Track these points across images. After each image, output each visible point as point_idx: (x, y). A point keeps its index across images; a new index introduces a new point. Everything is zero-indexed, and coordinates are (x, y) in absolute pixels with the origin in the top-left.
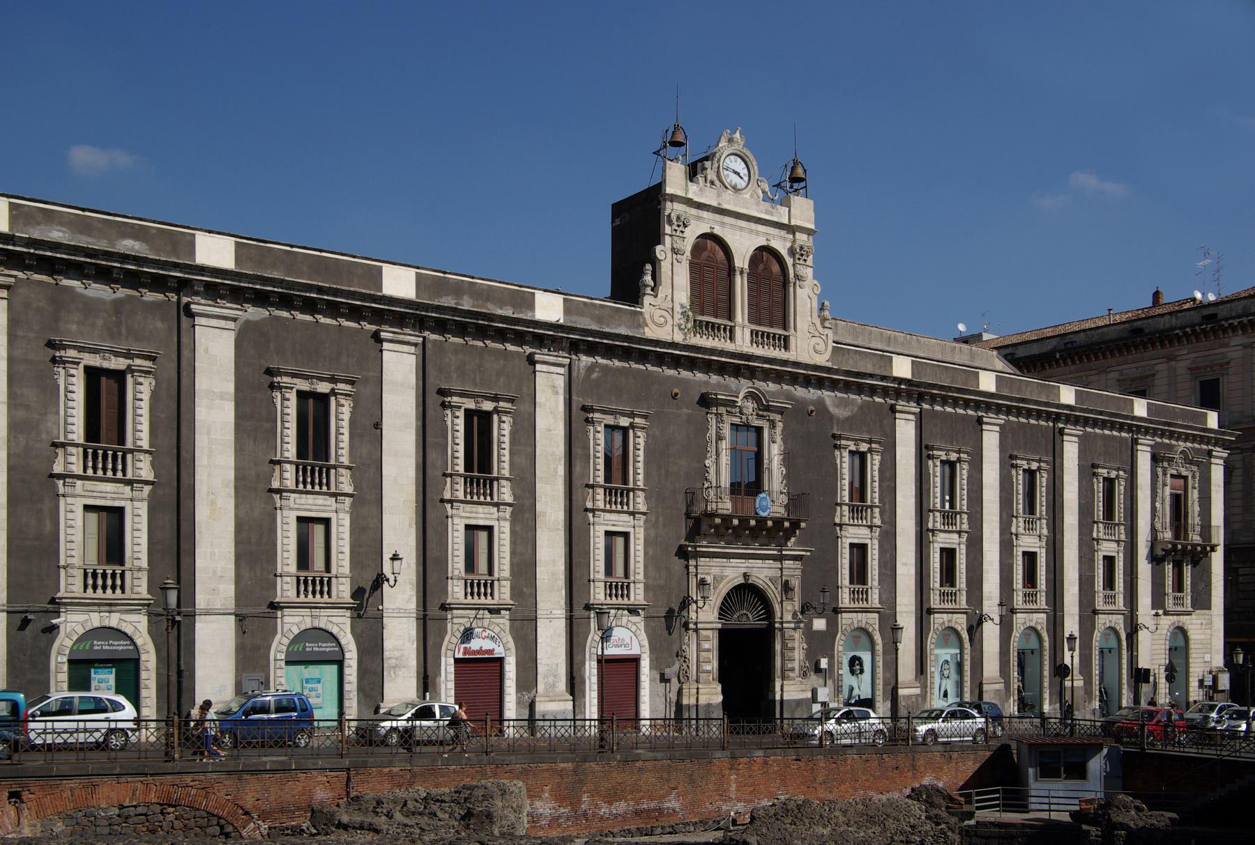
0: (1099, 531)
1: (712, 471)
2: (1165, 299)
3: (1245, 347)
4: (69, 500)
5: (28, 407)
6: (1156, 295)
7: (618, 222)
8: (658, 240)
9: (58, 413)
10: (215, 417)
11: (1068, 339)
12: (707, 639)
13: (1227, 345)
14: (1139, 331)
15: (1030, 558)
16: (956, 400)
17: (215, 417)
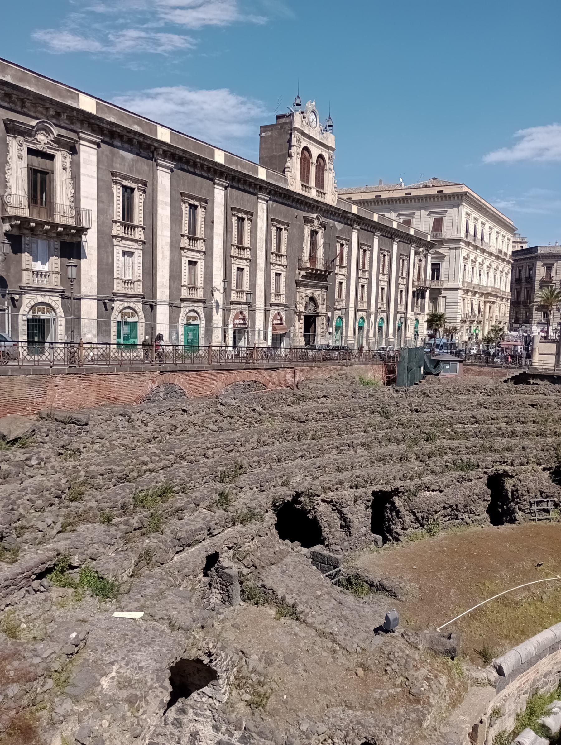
5: (103, 202)
9: (113, 206)
10: (164, 213)
17: (164, 213)
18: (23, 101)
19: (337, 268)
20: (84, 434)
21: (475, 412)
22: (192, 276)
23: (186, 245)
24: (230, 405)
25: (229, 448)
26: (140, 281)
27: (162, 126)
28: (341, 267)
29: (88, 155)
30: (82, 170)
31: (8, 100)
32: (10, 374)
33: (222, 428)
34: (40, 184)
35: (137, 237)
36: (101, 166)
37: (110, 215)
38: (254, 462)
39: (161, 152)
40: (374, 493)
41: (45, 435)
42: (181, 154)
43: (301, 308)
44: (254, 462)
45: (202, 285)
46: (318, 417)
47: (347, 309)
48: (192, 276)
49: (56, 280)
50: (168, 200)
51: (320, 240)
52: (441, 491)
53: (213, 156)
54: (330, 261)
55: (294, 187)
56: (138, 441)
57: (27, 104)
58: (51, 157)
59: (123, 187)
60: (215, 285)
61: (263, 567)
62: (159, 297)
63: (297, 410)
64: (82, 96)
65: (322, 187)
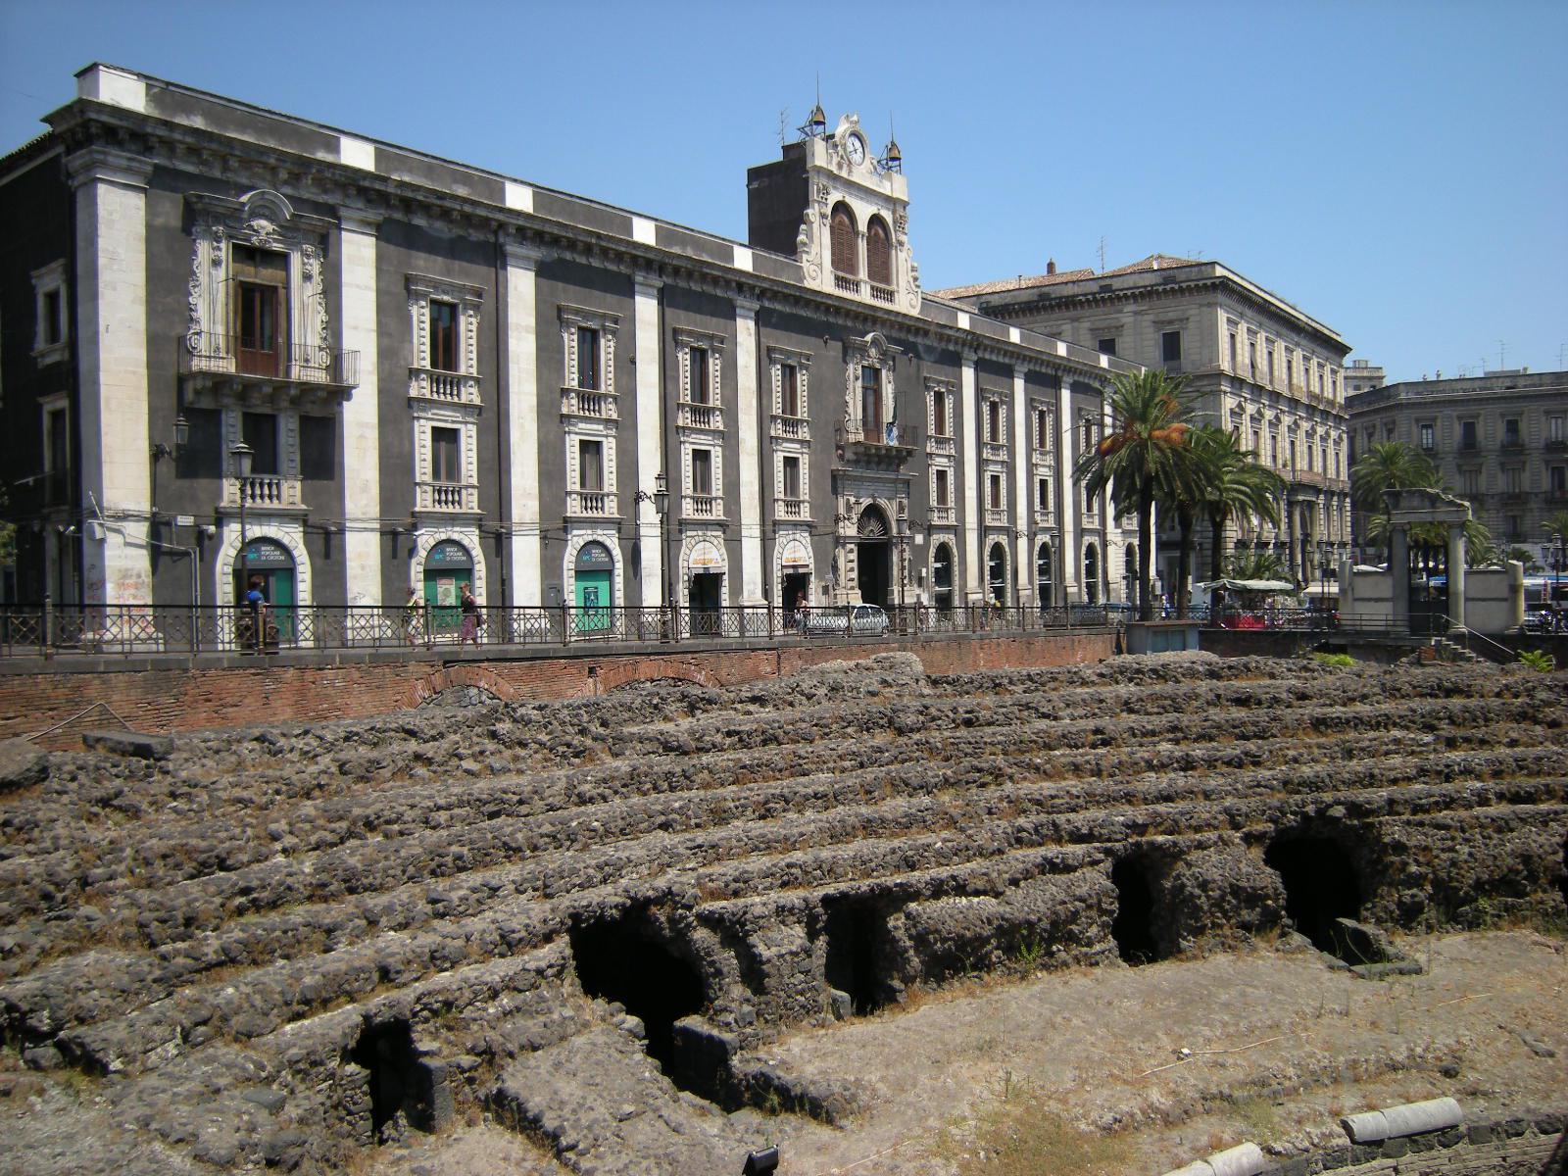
0: (1036, 458)
1: (851, 404)
2: (1058, 270)
3: (1135, 313)
4: (422, 422)
5: (390, 335)
6: (1051, 266)
7: (755, 185)
8: (806, 204)
9: (411, 342)
10: (522, 347)
11: (983, 299)
12: (851, 551)
13: (1121, 312)
14: (1043, 297)
15: (1043, 483)
16: (999, 350)
17: (522, 347)
18: (224, 160)
19: (931, 447)
20: (157, 777)
21: (1105, 722)
22: (702, 481)
23: (575, 408)
24: (530, 721)
25: (491, 808)
26: (473, 487)
27: (515, 181)
28: (940, 442)
29: (359, 252)
30: (346, 277)
31: (195, 160)
32: (102, 669)
33: (492, 769)
34: (258, 313)
35: (464, 399)
36: (385, 267)
37: (405, 359)
38: (542, 836)
39: (512, 231)
40: (826, 900)
41: (68, 777)
42: (556, 232)
43: (849, 529)
44: (542, 836)
45: (614, 489)
46: (728, 741)
47: (958, 530)
48: (702, 481)
49: (291, 492)
50: (532, 321)
51: (888, 390)
52: (997, 895)
53: (629, 230)
54: (912, 432)
55: (818, 281)
56: (278, 792)
57: (233, 163)
58: (282, 260)
59: (433, 302)
60: (1019, 528)
61: (511, 1055)
62: (515, 518)
63: (680, 727)
64: (346, 143)
65: (887, 279)
